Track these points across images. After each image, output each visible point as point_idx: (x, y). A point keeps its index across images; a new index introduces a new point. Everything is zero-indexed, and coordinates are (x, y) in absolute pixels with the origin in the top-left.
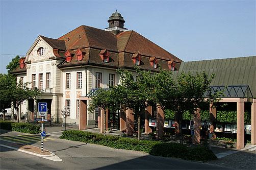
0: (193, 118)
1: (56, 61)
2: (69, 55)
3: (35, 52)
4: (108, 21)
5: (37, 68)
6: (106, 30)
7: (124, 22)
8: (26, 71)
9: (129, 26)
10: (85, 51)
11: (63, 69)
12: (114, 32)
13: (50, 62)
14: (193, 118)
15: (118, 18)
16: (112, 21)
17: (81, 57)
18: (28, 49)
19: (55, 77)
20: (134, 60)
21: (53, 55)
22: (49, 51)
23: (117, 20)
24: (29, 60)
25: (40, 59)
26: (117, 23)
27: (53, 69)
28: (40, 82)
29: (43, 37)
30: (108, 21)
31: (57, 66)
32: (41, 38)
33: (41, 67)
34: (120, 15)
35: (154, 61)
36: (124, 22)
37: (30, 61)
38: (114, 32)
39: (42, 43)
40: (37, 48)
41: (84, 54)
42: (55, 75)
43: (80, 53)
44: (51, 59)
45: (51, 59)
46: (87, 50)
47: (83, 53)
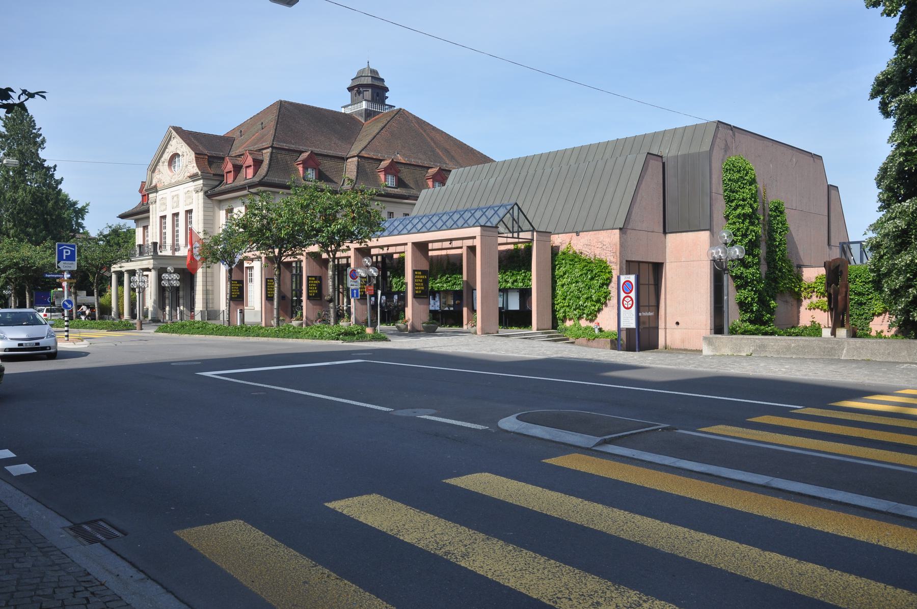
0: (562, 311)
1: (201, 182)
2: (229, 167)
3: (163, 167)
4: (350, 89)
5: (169, 202)
6: (343, 111)
7: (387, 90)
8: (148, 211)
9: (394, 99)
10: (260, 158)
11: (220, 201)
12: (361, 115)
13: (192, 186)
14: (562, 311)
15: (369, 81)
16: (356, 89)
17: (250, 172)
18: (149, 160)
19: (201, 217)
20: (382, 176)
21: (194, 169)
22: (188, 162)
23: (372, 87)
24: (153, 184)
25: (173, 181)
26: (368, 94)
27: (197, 202)
28: (162, 235)
29: (178, 130)
30: (350, 89)
31: (206, 193)
32: (174, 133)
33: (175, 199)
34: (374, 75)
35: (387, 171)
36: (387, 90)
37: (156, 186)
38: (359, 113)
39: (178, 145)
40: (167, 156)
41: (258, 163)
42: (201, 213)
43: (250, 161)
44: (194, 178)
45: (194, 178)
46: (266, 154)
47: (255, 160)
